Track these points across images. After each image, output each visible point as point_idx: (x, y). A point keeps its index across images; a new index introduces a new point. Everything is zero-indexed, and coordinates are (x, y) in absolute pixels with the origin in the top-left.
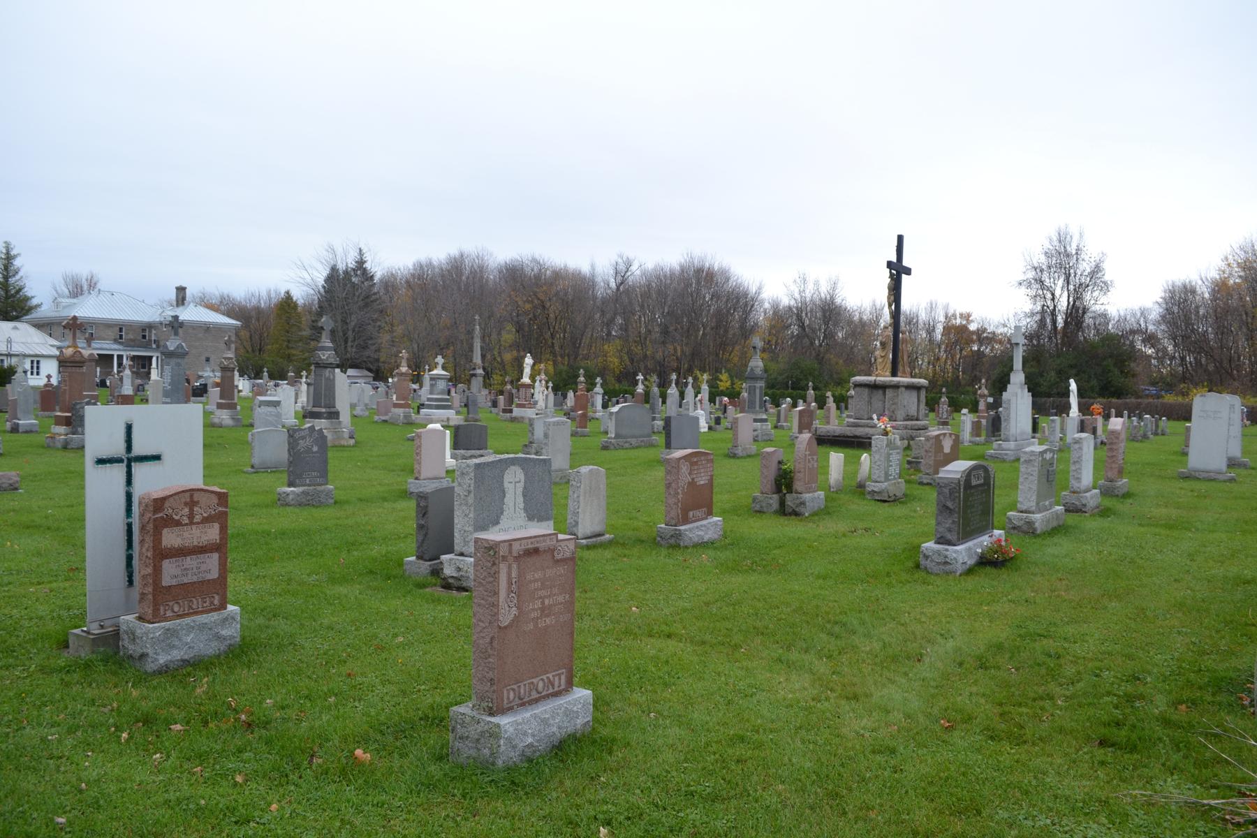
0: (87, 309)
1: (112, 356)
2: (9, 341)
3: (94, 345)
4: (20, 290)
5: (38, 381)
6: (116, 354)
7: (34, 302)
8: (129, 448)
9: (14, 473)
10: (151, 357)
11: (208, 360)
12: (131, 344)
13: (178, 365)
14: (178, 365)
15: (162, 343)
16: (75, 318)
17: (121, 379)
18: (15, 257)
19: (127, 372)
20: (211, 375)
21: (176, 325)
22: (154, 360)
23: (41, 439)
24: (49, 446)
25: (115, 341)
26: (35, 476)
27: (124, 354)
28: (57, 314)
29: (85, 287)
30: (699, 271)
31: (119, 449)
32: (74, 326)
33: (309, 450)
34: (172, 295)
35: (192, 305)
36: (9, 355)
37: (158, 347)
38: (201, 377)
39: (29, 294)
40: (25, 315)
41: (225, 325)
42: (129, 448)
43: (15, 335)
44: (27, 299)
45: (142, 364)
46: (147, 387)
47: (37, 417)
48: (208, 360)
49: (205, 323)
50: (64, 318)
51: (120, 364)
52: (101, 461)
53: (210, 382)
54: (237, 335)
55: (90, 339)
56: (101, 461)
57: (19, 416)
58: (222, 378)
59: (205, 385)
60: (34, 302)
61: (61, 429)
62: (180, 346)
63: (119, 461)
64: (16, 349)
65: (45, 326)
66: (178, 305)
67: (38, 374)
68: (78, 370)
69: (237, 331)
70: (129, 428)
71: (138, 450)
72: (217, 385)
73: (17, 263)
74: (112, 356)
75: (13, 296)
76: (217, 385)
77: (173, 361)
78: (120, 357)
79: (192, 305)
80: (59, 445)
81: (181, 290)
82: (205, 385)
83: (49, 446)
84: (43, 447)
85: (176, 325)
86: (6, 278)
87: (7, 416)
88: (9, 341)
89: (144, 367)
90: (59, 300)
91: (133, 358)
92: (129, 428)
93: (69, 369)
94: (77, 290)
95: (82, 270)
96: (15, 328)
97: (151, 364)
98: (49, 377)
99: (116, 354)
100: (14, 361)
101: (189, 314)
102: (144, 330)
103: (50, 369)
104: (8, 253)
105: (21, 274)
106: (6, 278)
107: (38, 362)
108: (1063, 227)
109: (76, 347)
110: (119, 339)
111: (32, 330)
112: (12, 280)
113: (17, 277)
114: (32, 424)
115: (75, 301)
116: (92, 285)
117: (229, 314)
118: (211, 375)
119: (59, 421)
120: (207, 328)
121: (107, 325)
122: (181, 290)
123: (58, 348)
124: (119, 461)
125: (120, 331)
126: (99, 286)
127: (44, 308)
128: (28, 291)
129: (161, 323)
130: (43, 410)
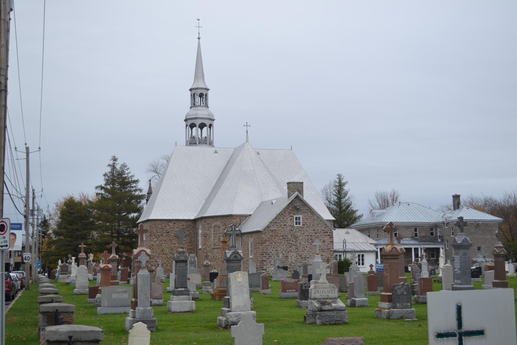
0: (393, 216)
1: (411, 249)
2: (344, 242)
3: (402, 242)
4: (348, 206)
5: (365, 269)
6: (413, 247)
7: (358, 214)
8: (460, 324)
9: (360, 338)
10: (438, 250)
11: (479, 249)
12: (423, 240)
13: (465, 254)
14: (465, 254)
15: (445, 238)
16: (391, 224)
17: (420, 266)
18: (344, 184)
19: (425, 261)
20: (483, 260)
21: (461, 223)
22: (441, 250)
23: (371, 311)
24: (378, 317)
25: (413, 238)
26: (372, 339)
27: (419, 247)
28: (373, 221)
29: (390, 201)
30: (66, 204)
31: (451, 325)
32: (392, 230)
33: (402, 294)
34: (450, 201)
35: (465, 208)
36: (345, 252)
37: (442, 240)
38: (476, 262)
39: (354, 209)
40: (352, 223)
41: (484, 221)
42: (460, 324)
43: (348, 238)
44: (354, 212)
45: (433, 255)
46: (437, 271)
47: (366, 295)
48: (479, 249)
49: (475, 221)
50: (383, 224)
51: (417, 256)
52: (440, 336)
53: (483, 266)
54: (499, 228)
55: (399, 239)
56: (440, 336)
57: (355, 295)
58: (495, 262)
59: (480, 268)
60: (358, 214)
61: (385, 305)
62: (465, 240)
63: (453, 335)
64: (349, 247)
65: (365, 230)
66: (455, 209)
67: (363, 264)
68: (395, 261)
69: (500, 225)
70: (459, 309)
71: (467, 326)
72: (490, 268)
73: (346, 188)
74: (411, 249)
75: (345, 211)
76: (490, 268)
77: (461, 252)
78: (416, 250)
79: (465, 208)
80: (384, 316)
81: (456, 197)
82: (480, 268)
83: (377, 317)
84: (374, 318)
85: (461, 224)
86: (340, 199)
87: (347, 295)
88: (344, 242)
89: (433, 256)
90: (374, 211)
91: (426, 250)
92: (459, 309)
93: (389, 261)
94: (386, 202)
95: (387, 189)
96: (347, 233)
97: (438, 256)
98: (371, 266)
99: (413, 247)
100: (349, 256)
101: (469, 214)
102: (432, 229)
103: (370, 260)
104: (340, 182)
105: (348, 195)
106: (340, 199)
107: (363, 256)
108: (81, 193)
109: (392, 244)
110: (415, 237)
111: (358, 234)
112: (343, 200)
113: (347, 198)
114: (364, 301)
115: (384, 211)
116: (395, 199)
117: (492, 213)
118: (483, 260)
119: (384, 299)
120: (478, 225)
121: (407, 226)
122: (456, 197)
123: (376, 245)
124: (453, 335)
125: (416, 230)
126: (399, 199)
127: (364, 217)
128: (354, 207)
129: (444, 223)
130: (370, 290)
